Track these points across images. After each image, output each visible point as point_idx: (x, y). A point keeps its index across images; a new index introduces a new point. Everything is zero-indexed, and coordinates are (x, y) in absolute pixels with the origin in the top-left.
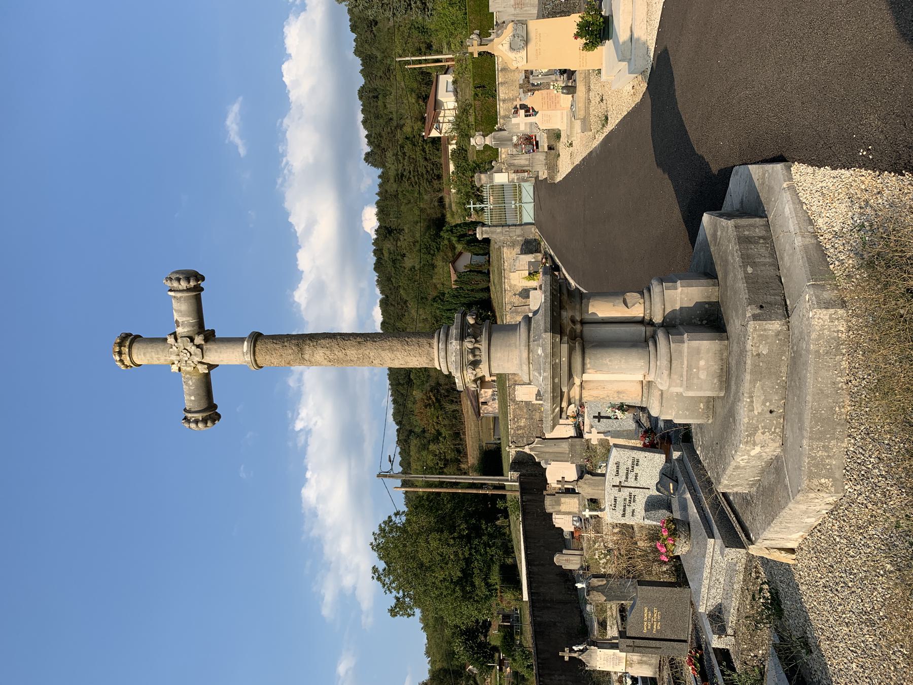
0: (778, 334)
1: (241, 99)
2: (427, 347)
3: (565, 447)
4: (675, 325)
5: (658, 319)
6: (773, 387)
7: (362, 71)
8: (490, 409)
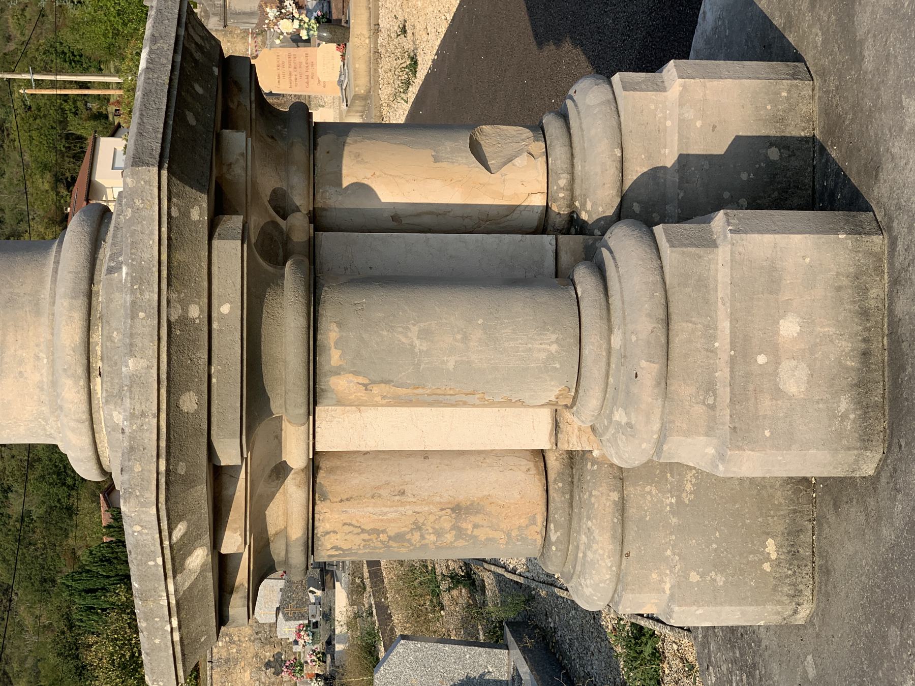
4: (671, 201)
5: (598, 202)
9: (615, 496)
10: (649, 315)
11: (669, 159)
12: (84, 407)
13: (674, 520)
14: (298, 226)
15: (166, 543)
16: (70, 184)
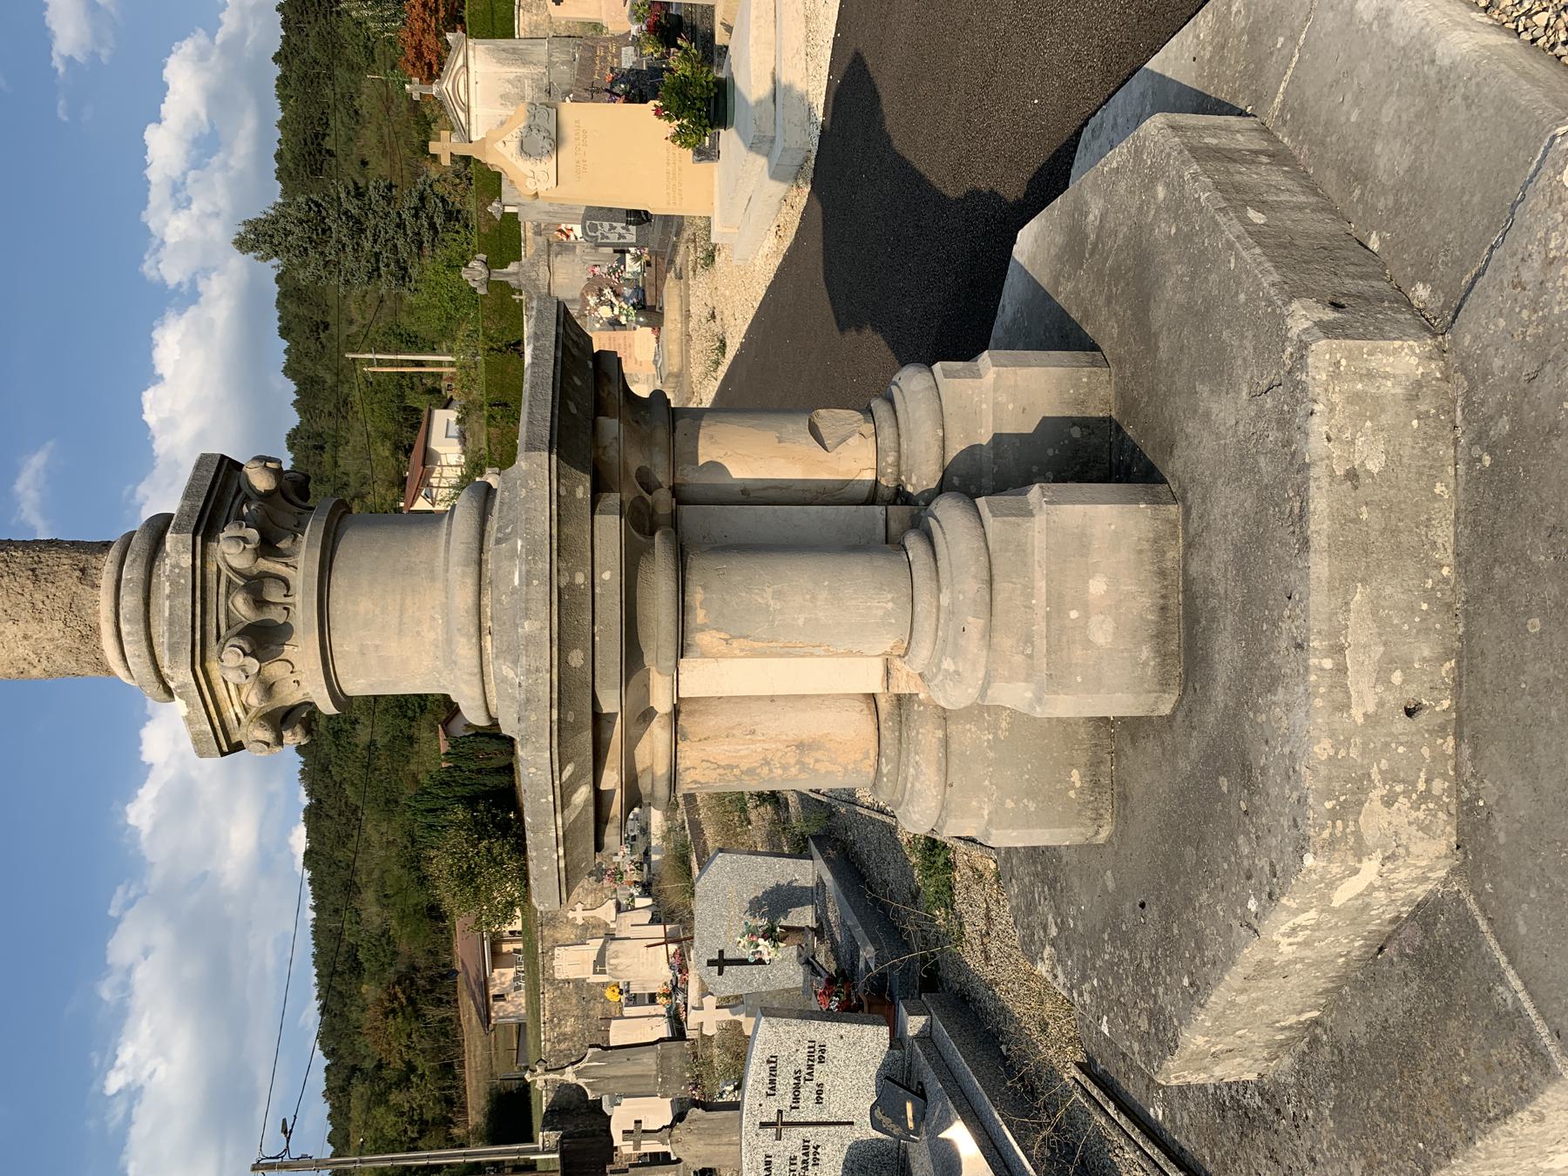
0: (1415, 391)
1: (50, 444)
2: (69, 580)
3: (649, 1061)
5: (922, 477)
6: (1412, 609)
7: (295, 403)
8: (511, 1008)
9: (940, 733)
10: (975, 577)
11: (984, 438)
12: (476, 661)
13: (991, 755)
14: (662, 501)
15: (557, 782)
16: (408, 450)
